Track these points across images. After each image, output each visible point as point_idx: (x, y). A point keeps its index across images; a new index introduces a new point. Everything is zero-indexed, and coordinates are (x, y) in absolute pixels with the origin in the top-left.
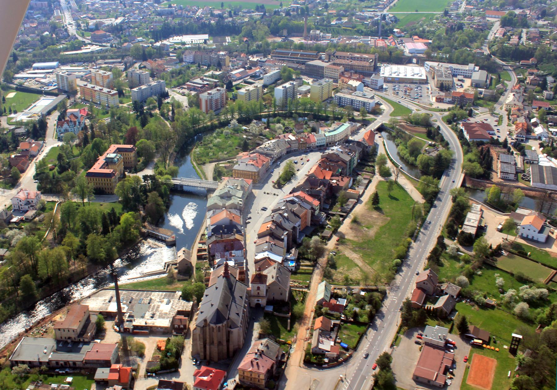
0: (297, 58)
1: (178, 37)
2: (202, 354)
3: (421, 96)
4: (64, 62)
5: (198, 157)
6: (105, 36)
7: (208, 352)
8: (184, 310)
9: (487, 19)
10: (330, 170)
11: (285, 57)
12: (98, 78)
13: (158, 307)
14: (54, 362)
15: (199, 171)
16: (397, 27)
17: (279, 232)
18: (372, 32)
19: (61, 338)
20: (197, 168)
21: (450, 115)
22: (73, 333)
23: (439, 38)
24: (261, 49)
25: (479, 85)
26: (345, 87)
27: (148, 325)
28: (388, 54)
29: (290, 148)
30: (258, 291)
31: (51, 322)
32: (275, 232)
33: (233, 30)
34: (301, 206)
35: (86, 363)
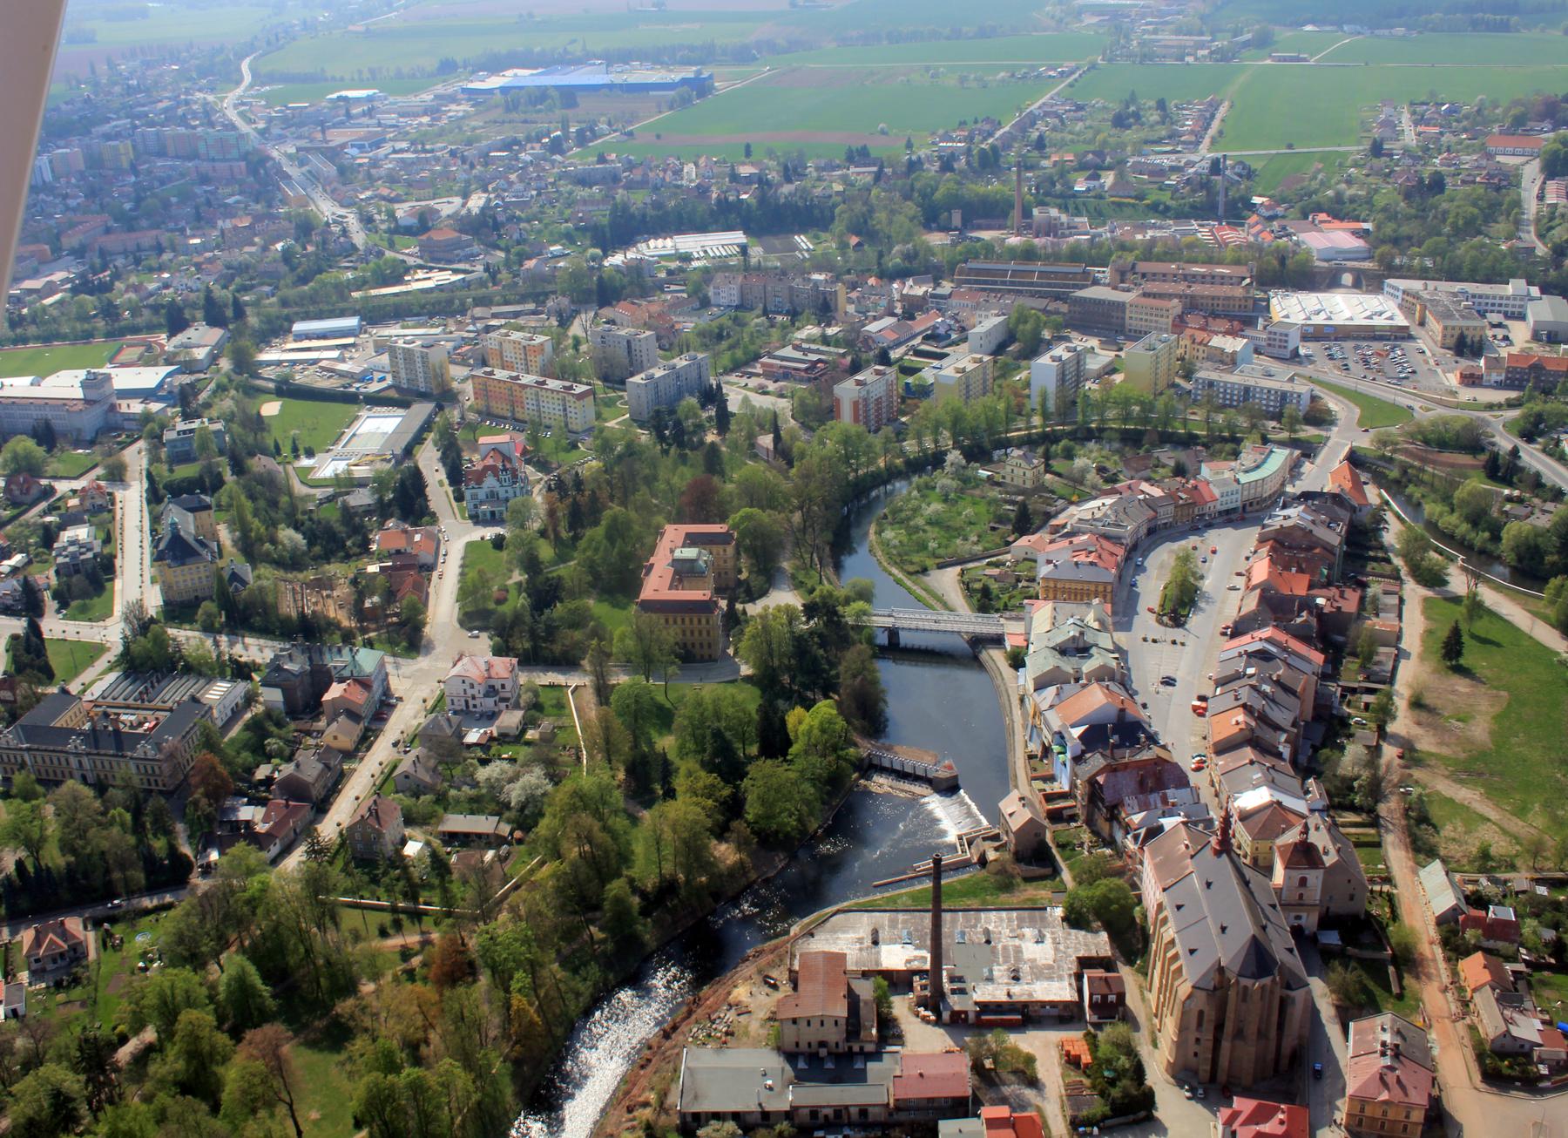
0: (1031, 284)
1: (660, 242)
2: (1206, 1068)
3: (1414, 372)
4: (375, 315)
5: (900, 555)
6: (458, 245)
7: (1224, 1061)
8: (1094, 954)
9: (1499, 158)
10: (1300, 570)
11: (995, 283)
12: (509, 354)
13: (1018, 950)
14: (807, 1111)
15: (919, 591)
16: (1260, 190)
17: (1267, 735)
18: (1193, 207)
19: (797, 1044)
20: (909, 583)
21: (1525, 417)
22: (834, 1029)
23: (1390, 214)
24: (915, 264)
25: (1556, 334)
26: (1201, 355)
27: (1015, 999)
28: (1275, 263)
29: (1155, 518)
30: (1301, 891)
31: (730, 1006)
32: (1258, 733)
33: (812, 217)
34: (1289, 665)
35: (898, 1109)
